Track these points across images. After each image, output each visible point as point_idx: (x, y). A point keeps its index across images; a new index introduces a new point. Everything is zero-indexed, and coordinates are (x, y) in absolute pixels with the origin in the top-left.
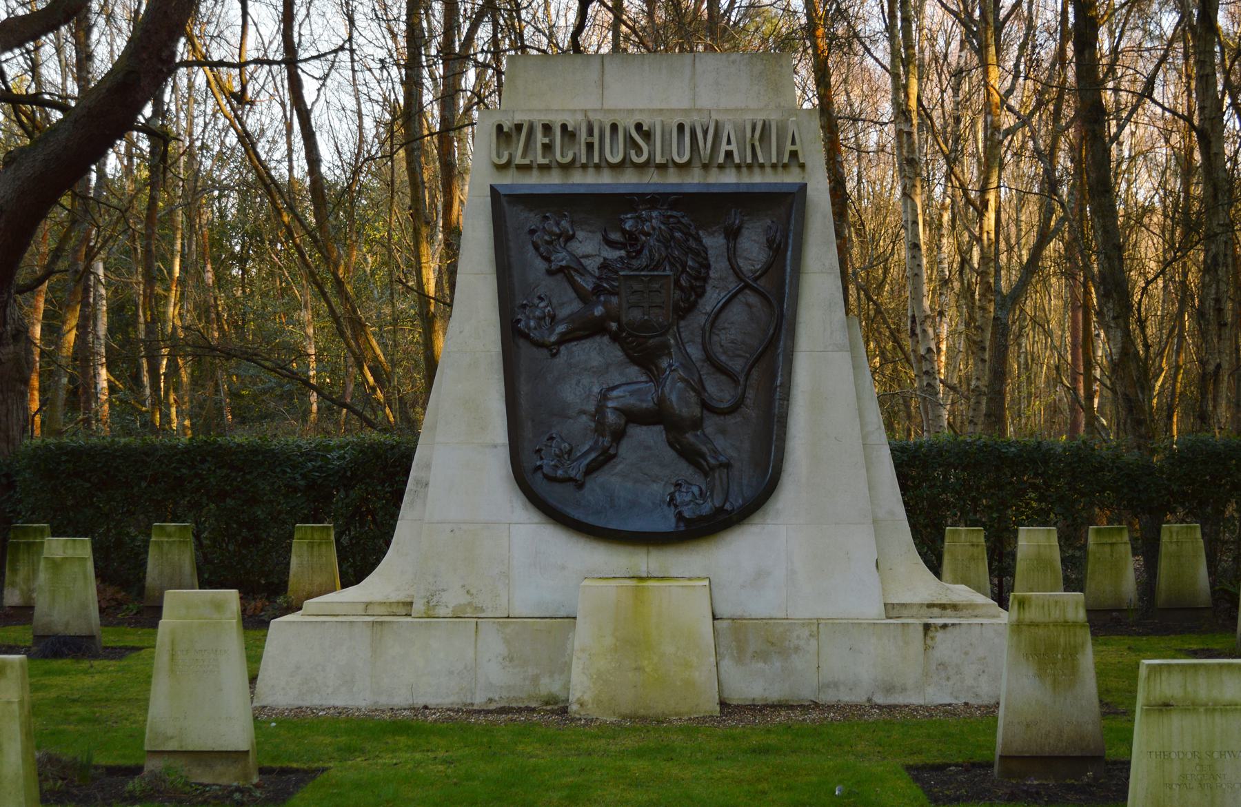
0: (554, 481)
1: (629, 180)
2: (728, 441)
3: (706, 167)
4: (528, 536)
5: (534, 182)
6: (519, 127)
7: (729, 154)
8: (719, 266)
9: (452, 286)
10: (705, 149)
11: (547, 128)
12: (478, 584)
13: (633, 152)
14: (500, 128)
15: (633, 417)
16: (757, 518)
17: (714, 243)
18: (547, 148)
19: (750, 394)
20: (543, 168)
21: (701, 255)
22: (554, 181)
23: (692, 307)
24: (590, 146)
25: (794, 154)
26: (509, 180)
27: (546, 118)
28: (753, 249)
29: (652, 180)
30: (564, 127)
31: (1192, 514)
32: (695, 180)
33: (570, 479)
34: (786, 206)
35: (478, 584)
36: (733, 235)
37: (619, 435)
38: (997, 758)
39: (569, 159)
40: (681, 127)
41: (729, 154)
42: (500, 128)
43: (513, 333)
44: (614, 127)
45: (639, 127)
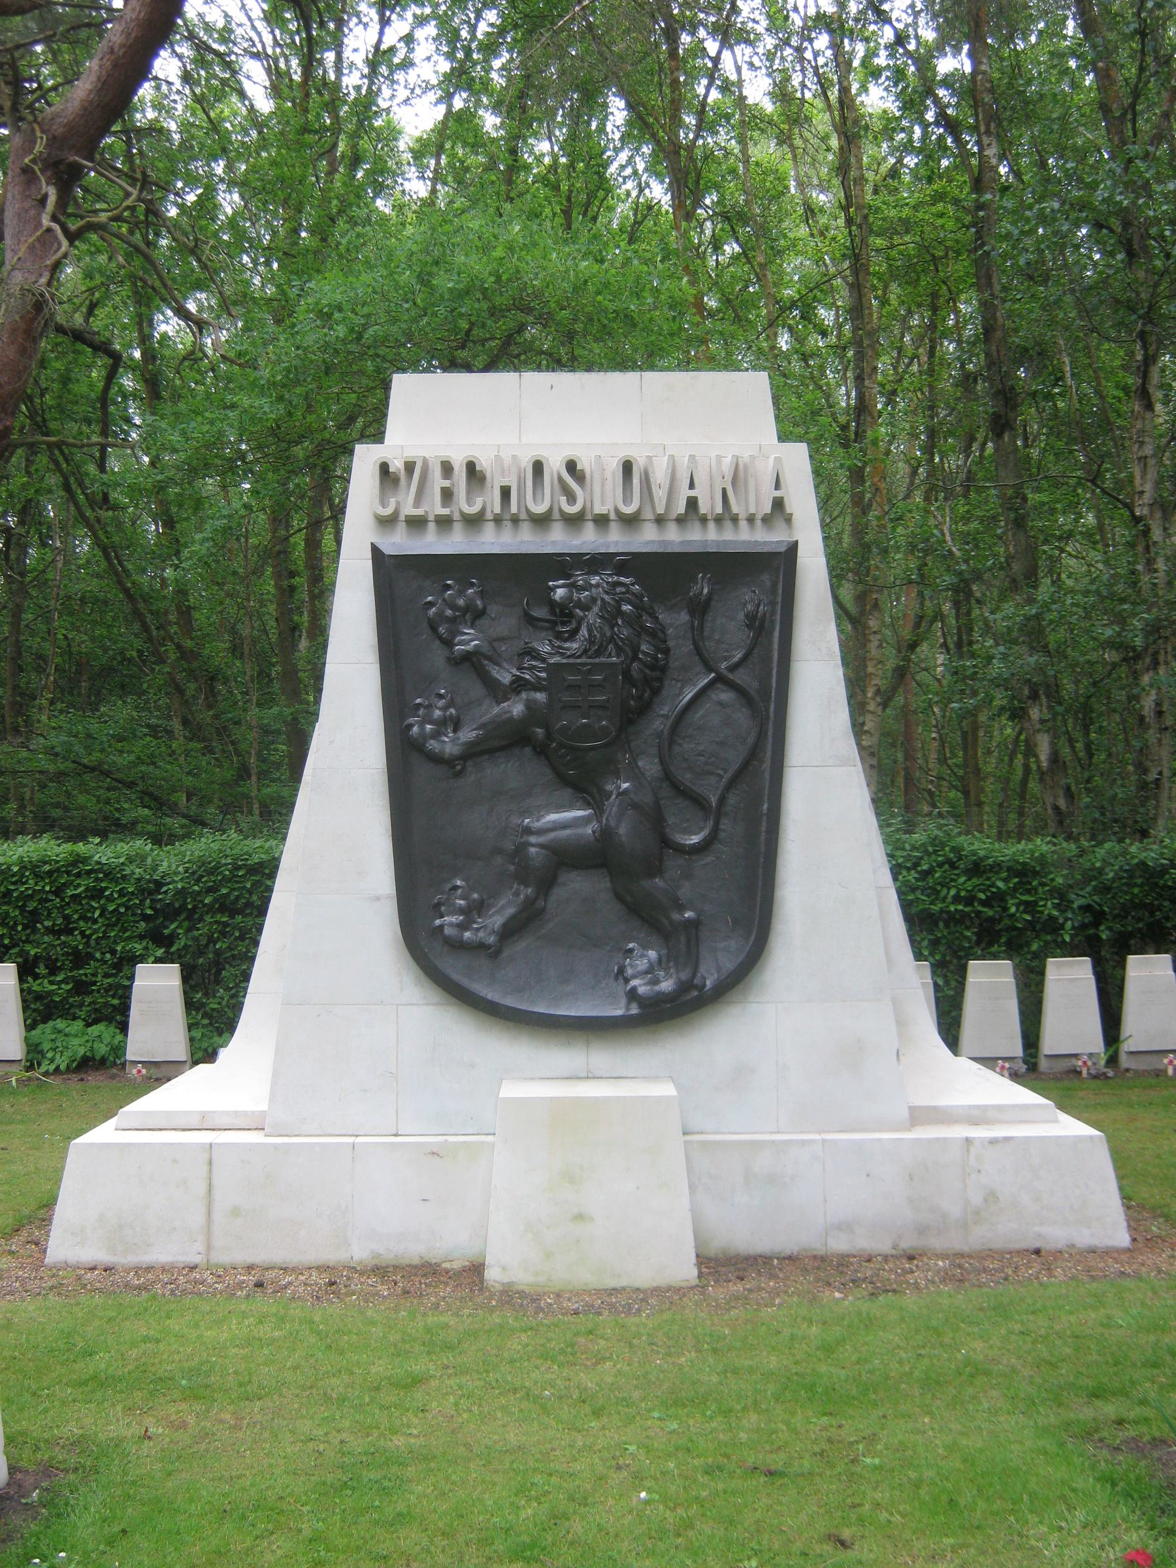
1: (557, 540)
2: (694, 891)
3: (660, 520)
5: (432, 543)
7: (692, 503)
8: (681, 648)
10: (660, 495)
11: (447, 469)
13: (563, 499)
14: (384, 468)
15: (566, 858)
16: (433, 994)
17: (675, 620)
18: (447, 495)
20: (444, 523)
21: (658, 636)
22: (456, 543)
23: (645, 709)
24: (506, 492)
25: (778, 504)
26: (399, 543)
29: (588, 540)
30: (471, 467)
32: (648, 539)
34: (784, 562)
36: (700, 609)
37: (546, 884)
40: (627, 467)
41: (692, 503)
43: (405, 753)
44: (538, 468)
45: (571, 466)
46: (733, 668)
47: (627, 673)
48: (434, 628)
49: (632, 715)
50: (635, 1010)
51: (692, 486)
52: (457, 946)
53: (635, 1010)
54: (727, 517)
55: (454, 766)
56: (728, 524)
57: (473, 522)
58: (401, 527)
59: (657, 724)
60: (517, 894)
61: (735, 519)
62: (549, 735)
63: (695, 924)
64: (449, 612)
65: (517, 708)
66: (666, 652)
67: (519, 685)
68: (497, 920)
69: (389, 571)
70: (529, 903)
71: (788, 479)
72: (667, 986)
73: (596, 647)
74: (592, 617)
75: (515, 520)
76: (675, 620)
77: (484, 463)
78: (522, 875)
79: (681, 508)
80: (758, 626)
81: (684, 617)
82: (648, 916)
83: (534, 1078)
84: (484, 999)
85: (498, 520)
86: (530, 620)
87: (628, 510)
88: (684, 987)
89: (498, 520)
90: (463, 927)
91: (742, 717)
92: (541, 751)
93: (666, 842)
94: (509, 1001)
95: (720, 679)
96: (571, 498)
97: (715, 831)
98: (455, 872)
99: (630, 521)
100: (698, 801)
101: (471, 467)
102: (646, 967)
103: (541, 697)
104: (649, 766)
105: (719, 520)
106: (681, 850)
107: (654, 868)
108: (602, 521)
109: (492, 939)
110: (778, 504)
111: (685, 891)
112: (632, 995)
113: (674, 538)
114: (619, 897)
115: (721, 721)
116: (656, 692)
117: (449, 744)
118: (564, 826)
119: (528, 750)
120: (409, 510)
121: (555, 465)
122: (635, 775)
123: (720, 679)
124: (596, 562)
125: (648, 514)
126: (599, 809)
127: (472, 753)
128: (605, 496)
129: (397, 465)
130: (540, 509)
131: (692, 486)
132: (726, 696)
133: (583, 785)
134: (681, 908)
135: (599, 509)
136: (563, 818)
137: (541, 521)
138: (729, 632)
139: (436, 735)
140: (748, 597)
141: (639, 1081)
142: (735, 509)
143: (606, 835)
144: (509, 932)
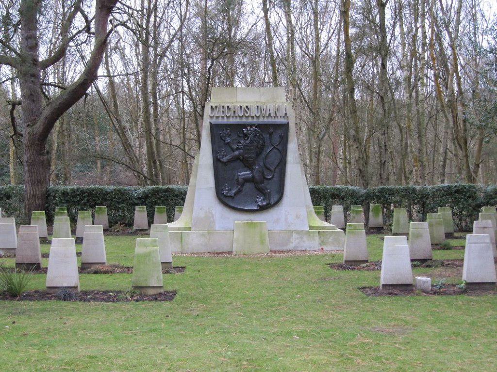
0: (227, 197)
1: (244, 120)
2: (271, 187)
4: (218, 210)
5: (220, 121)
6: (216, 107)
7: (270, 114)
9: (155, 299)
12: (203, 218)
13: (245, 113)
14: (212, 107)
15: (246, 180)
16: (222, 205)
17: (266, 136)
18: (223, 112)
19: (276, 174)
20: (223, 117)
21: (263, 139)
22: (225, 121)
23: (261, 153)
24: (234, 112)
25: (286, 114)
26: (214, 121)
27: (223, 105)
28: (276, 139)
30: (228, 107)
31: (163, 203)
32: (261, 120)
33: (231, 196)
35: (203, 218)
36: (271, 134)
37: (243, 185)
38: (381, 286)
39: (229, 115)
40: (258, 107)
41: (270, 114)
42: (212, 107)
44: (241, 107)
45: (247, 107)
46: (277, 145)
47: (257, 147)
48: (221, 138)
49: (258, 155)
50: (259, 208)
51: (269, 111)
52: (226, 196)
53: (259, 208)
54: (276, 116)
55: (225, 164)
56: (276, 118)
57: (228, 117)
58: (215, 118)
59: (263, 156)
60: (237, 187)
61: (278, 117)
62: (243, 158)
63: (270, 192)
64: (224, 135)
65: (237, 153)
66: (264, 142)
67: (237, 149)
68: (234, 192)
69: (214, 128)
70: (239, 189)
71: (287, 109)
72: (264, 204)
73: (252, 142)
74: (251, 136)
75: (236, 117)
76: (266, 136)
77: (230, 106)
78: (238, 184)
79: (267, 115)
80: (281, 137)
81: (268, 136)
82: (261, 191)
83: (240, 219)
84: (246, 210)
85: (233, 117)
86: (239, 136)
87: (258, 115)
88: (268, 204)
89: (233, 117)
90: (228, 193)
91: (279, 155)
92: (241, 161)
93: (265, 178)
94: (236, 206)
95: (275, 147)
96: (247, 113)
97: (273, 176)
98: (226, 183)
99: (258, 117)
100: (270, 170)
101: (228, 107)
102: (261, 201)
103: (241, 151)
104: (261, 164)
105: (274, 117)
106: (267, 179)
107: (262, 182)
108: (252, 117)
109: (233, 195)
110: (286, 114)
111: (268, 186)
112: (258, 205)
113: (266, 121)
114: (256, 187)
115: (274, 158)
116: (262, 150)
117: (225, 159)
118: (246, 174)
119: (239, 160)
120: (217, 115)
121: (244, 106)
122: (259, 165)
123: (275, 147)
124: (252, 125)
125: (261, 116)
126: (252, 172)
127: (229, 161)
128: (253, 112)
129: (214, 106)
130: (241, 115)
131: (269, 111)
132: (275, 150)
133: (248, 166)
134: (267, 189)
135: (252, 115)
136: (245, 173)
137: (241, 117)
138: (276, 139)
139: (222, 158)
140: (280, 132)
141: (264, 219)
142: (278, 115)
143: (253, 176)
144: (236, 194)
